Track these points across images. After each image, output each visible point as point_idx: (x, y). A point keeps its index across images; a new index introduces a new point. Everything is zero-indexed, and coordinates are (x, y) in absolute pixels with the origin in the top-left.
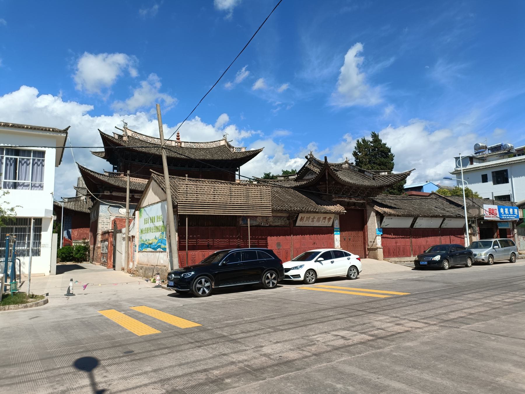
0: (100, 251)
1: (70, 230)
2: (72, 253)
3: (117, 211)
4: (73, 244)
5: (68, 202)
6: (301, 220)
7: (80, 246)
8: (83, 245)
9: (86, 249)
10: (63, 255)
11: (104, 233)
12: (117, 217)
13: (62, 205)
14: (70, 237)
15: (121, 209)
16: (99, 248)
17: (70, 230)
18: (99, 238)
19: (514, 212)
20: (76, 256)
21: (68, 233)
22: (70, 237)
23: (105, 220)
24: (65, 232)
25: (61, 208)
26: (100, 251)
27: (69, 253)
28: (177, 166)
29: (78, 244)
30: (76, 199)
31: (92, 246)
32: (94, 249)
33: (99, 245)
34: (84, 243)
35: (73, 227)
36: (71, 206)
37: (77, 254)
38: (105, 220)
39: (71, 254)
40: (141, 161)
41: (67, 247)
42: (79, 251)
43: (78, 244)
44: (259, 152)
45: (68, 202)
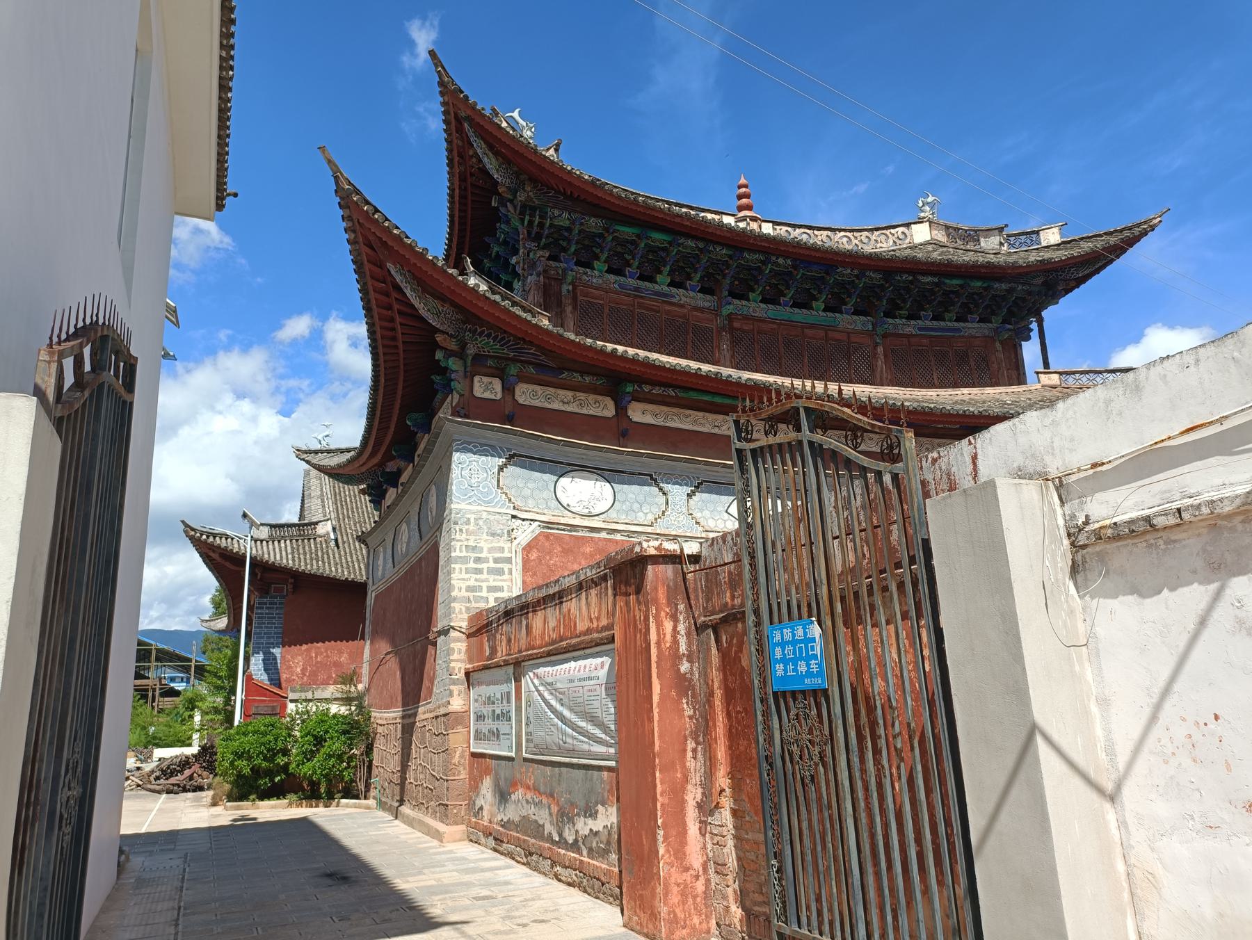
0: (462, 743)
1: (277, 651)
2: (285, 752)
3: (548, 494)
4: (291, 707)
5: (272, 539)
6: (509, 693)
7: (324, 717)
8: (334, 709)
9: (356, 730)
10: (241, 763)
11: (483, 627)
12: (547, 525)
13: (249, 549)
14: (276, 680)
15: (565, 481)
16: (457, 719)
17: (277, 651)
18: (454, 654)
19: (808, 665)
20: (306, 769)
21: (270, 665)
22: (276, 680)
23: (485, 543)
24: (257, 661)
25: (239, 560)
26: (462, 743)
27: (271, 755)
28: (774, 302)
29: (312, 707)
30: (303, 529)
31: (386, 718)
32: (408, 730)
33: (457, 704)
34: (347, 700)
35: (290, 639)
36: (281, 554)
37: (309, 756)
38: (485, 543)
39: (281, 760)
40: (618, 272)
41: (259, 723)
42: (319, 741)
43: (312, 707)
44: (1144, 233)
45: (272, 539)
